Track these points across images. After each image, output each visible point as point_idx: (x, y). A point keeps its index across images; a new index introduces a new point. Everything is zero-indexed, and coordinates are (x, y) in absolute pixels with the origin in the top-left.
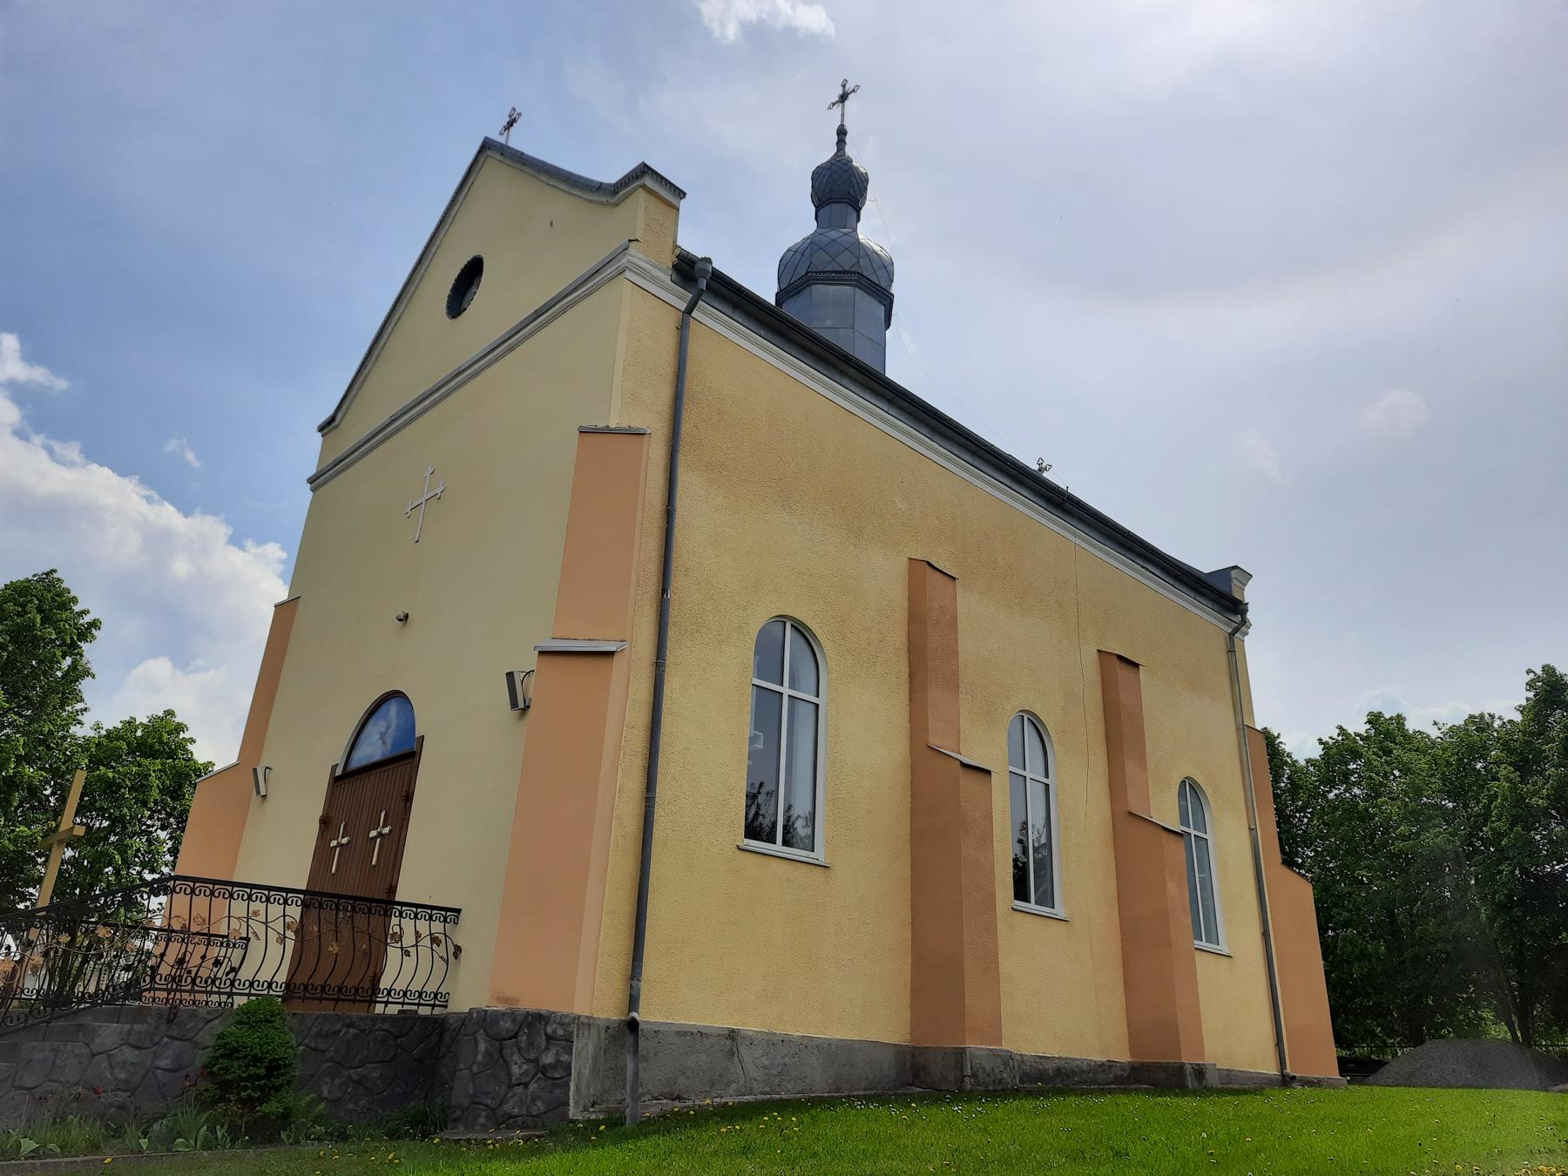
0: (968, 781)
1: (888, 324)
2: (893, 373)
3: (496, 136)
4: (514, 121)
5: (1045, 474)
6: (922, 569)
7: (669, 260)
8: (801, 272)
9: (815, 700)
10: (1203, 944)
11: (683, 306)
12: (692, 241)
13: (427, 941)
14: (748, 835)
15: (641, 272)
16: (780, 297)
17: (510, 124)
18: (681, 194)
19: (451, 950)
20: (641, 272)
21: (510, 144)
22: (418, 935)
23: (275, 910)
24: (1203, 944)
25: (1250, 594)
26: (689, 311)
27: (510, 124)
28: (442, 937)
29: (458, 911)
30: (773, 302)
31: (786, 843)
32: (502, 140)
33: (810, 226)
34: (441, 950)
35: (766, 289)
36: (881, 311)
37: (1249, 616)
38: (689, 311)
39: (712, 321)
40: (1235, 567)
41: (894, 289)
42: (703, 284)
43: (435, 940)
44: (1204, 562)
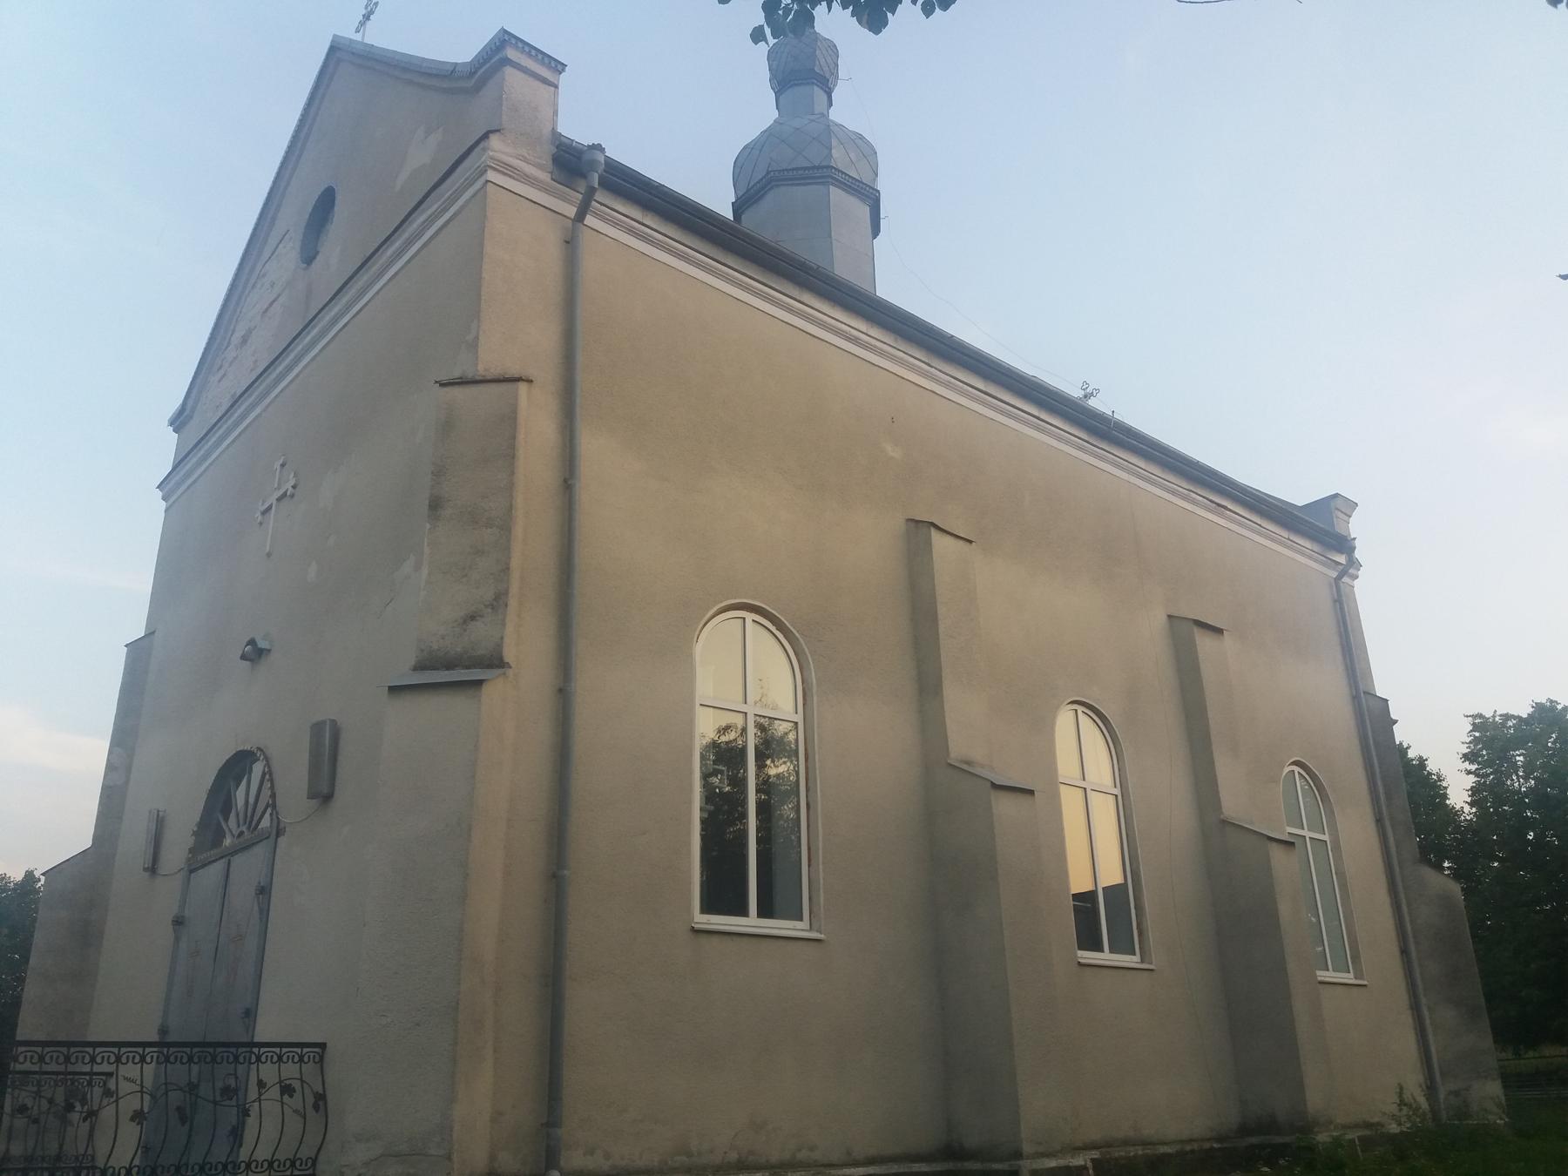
0: (1005, 807)
1: (876, 230)
2: (890, 288)
3: (349, 33)
4: (371, 12)
5: (1093, 403)
6: (919, 530)
7: (546, 152)
8: (762, 175)
9: (744, 708)
10: (1105, 957)
11: (571, 211)
12: (577, 128)
13: (274, 1092)
14: (707, 908)
15: (508, 170)
16: (738, 208)
17: (367, 17)
18: (558, 67)
19: (310, 1100)
20: (508, 170)
21: (367, 41)
22: (261, 1084)
23: (130, 1070)
24: (1105, 957)
25: (1357, 527)
26: (580, 217)
27: (367, 17)
28: (296, 1084)
29: (323, 1046)
30: (729, 214)
31: (765, 911)
32: (358, 37)
33: (774, 114)
34: (295, 1102)
35: (719, 199)
36: (864, 211)
37: (1357, 554)
38: (580, 217)
39: (614, 233)
40: (1336, 495)
41: (882, 185)
42: (595, 180)
43: (287, 1090)
44: (1298, 492)
